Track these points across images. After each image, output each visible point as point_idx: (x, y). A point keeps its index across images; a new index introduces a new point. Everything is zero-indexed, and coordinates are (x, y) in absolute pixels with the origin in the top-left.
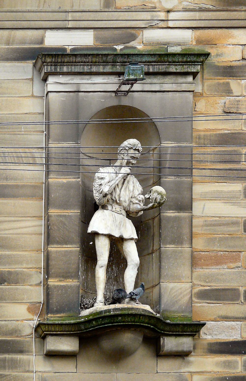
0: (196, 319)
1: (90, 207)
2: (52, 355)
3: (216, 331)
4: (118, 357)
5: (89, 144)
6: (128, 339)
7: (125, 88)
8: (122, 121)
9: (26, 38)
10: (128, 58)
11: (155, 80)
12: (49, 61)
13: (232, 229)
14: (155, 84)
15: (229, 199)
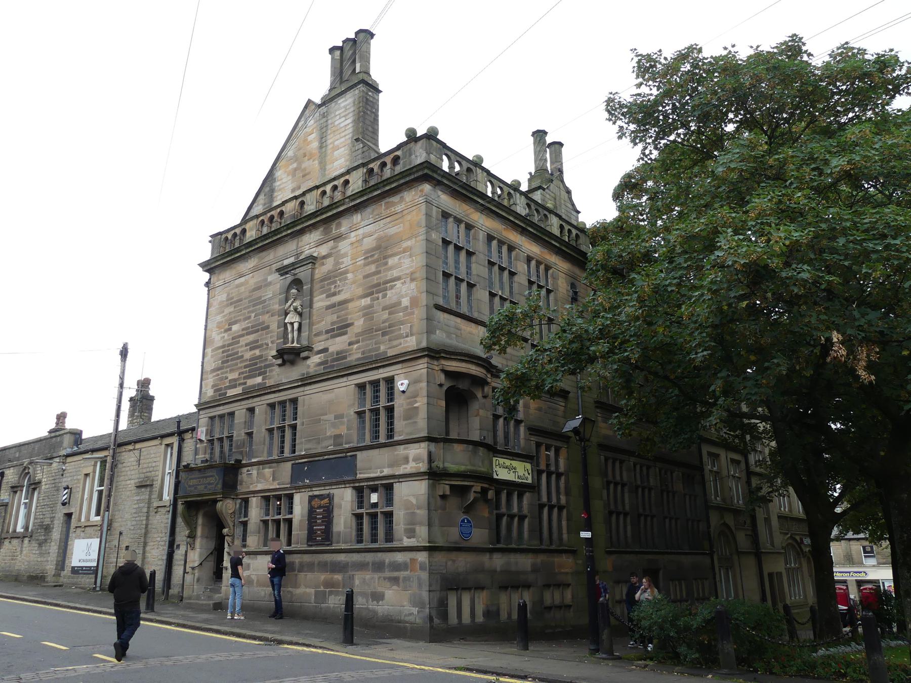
3: (318, 347)
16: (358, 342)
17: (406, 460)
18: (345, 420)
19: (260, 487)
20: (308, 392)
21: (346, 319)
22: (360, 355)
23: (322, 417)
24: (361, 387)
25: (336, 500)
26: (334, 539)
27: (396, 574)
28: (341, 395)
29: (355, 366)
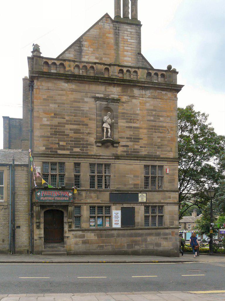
0: (119, 141)
1: (103, 123)
2: (98, 146)
3: (122, 143)
4: (107, 147)
5: (103, 113)
6: (109, 144)
7: (108, 104)
8: (107, 109)
9: (93, 95)
10: (109, 99)
11: (112, 103)
12: (97, 99)
13: (124, 127)
14: (113, 103)
15: (123, 123)
16: (145, 147)
17: (170, 198)
18: (140, 178)
19: (89, 201)
20: (117, 163)
21: (139, 136)
22: (146, 153)
23: (126, 175)
24: (146, 167)
25: (136, 210)
26: (136, 224)
27: (166, 237)
28: (138, 167)
29: (142, 157)
